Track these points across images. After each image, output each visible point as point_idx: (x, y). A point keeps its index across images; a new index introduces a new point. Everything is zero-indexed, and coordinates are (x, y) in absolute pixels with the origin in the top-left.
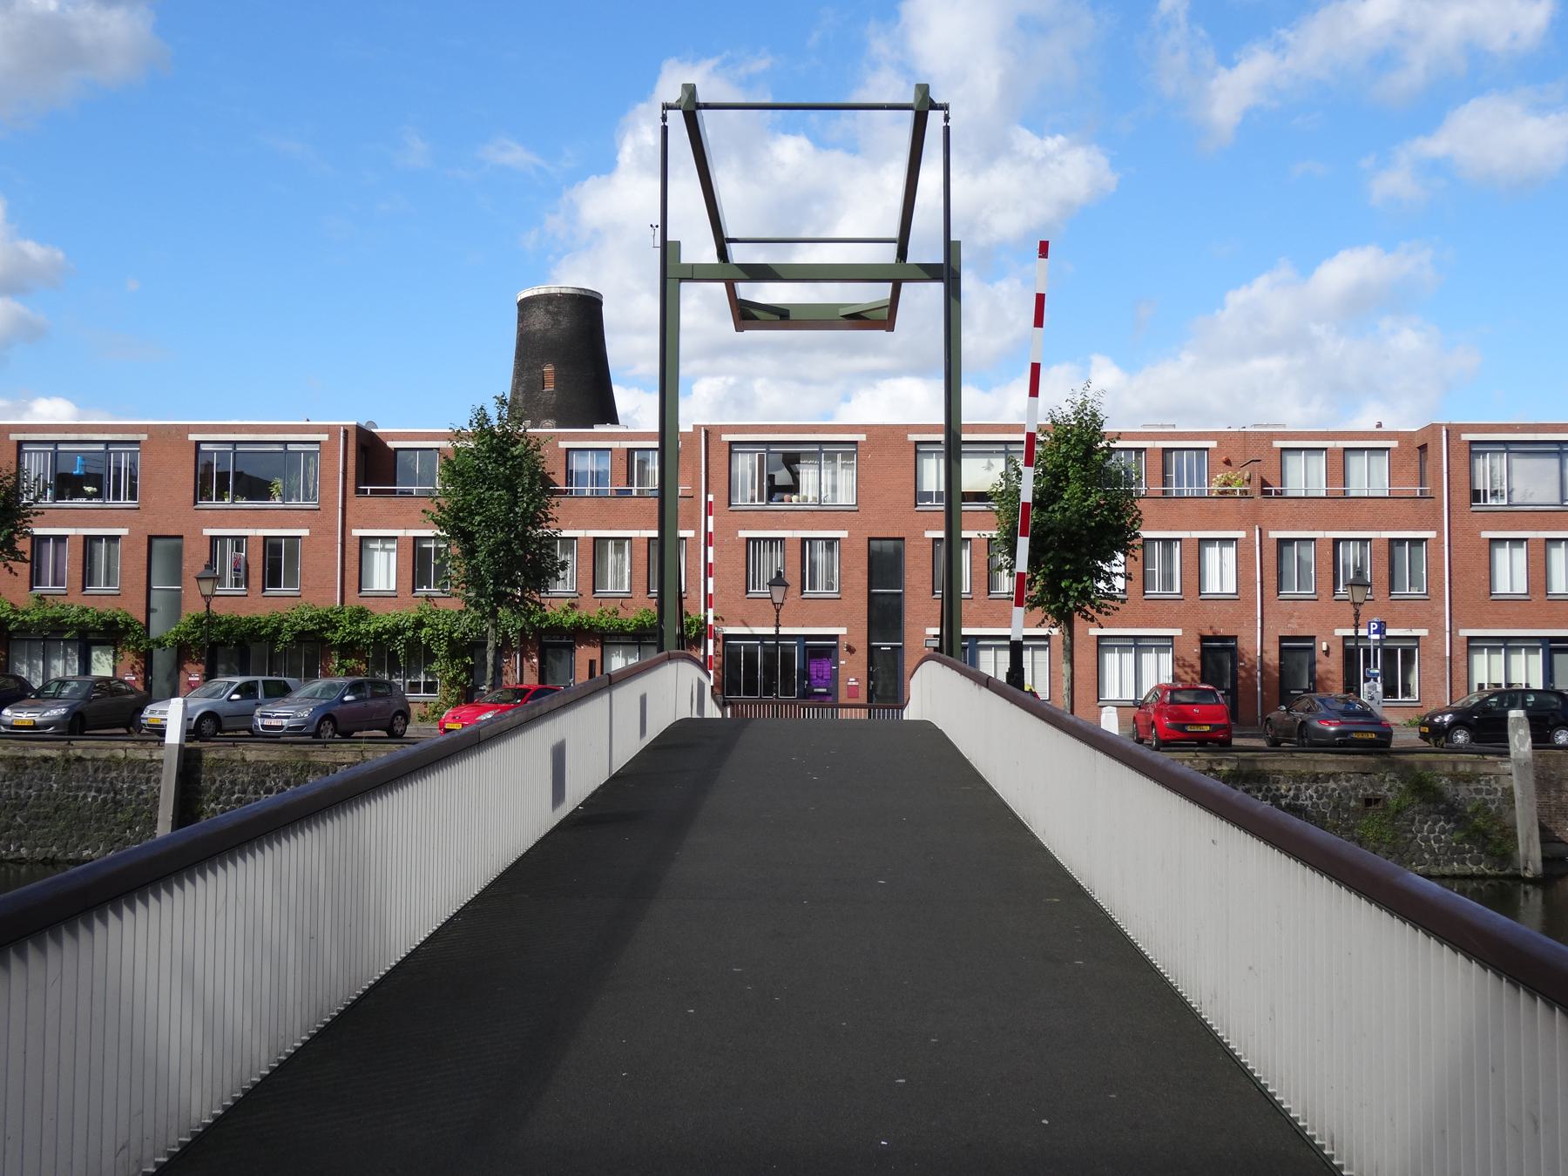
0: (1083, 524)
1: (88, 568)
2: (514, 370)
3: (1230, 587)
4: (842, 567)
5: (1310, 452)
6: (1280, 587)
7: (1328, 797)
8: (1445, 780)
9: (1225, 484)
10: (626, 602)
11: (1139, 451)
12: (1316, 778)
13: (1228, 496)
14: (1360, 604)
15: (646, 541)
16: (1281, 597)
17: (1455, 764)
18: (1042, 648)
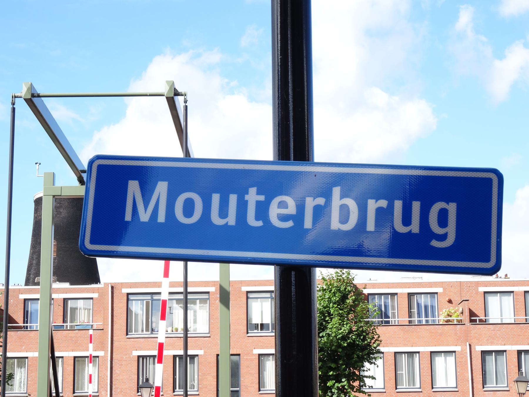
0: (339, 346)
2: (31, 244)
3: (452, 383)
4: (200, 374)
5: (502, 294)
6: (484, 383)
9: (449, 315)
11: (393, 295)
13: (450, 323)
14: (524, 394)
15: (73, 359)
16: (485, 389)
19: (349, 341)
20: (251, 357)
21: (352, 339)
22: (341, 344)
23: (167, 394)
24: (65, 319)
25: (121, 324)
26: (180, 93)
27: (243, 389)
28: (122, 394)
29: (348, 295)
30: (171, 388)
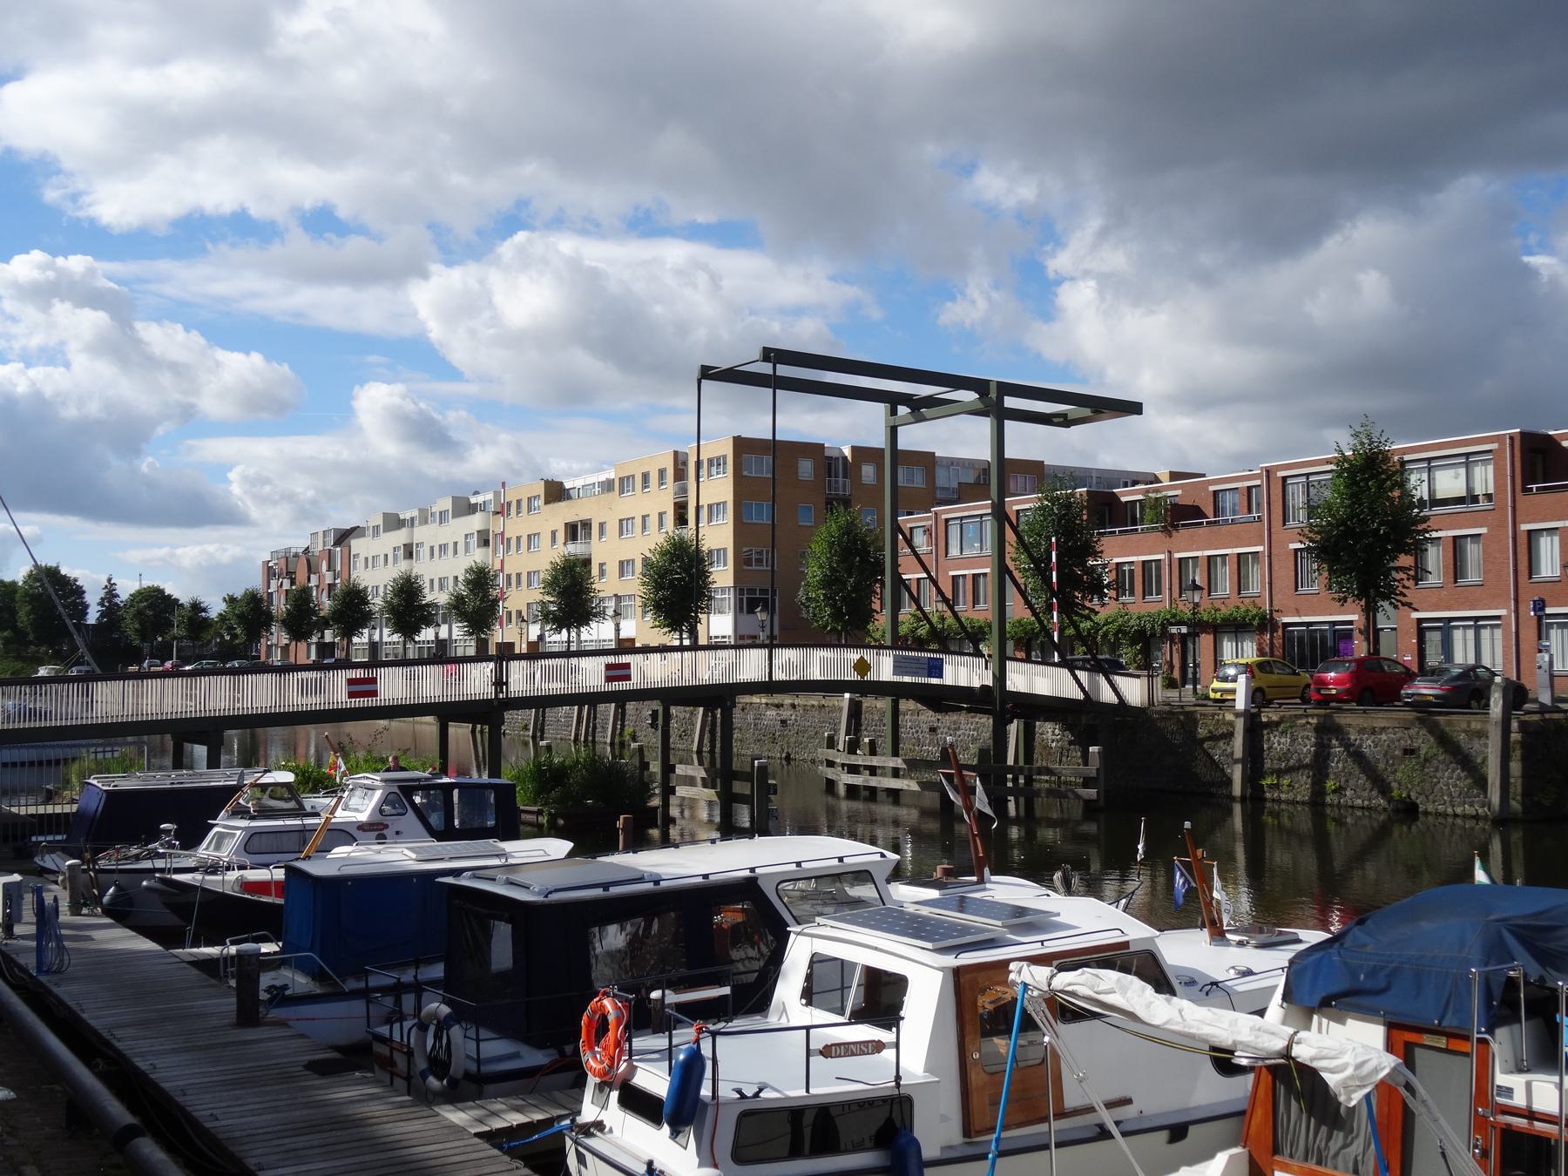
1: (1458, 564)
7: (1381, 746)
8: (1462, 736)
10: (1226, 601)
12: (1373, 731)
17: (1469, 723)
18: (1497, 626)
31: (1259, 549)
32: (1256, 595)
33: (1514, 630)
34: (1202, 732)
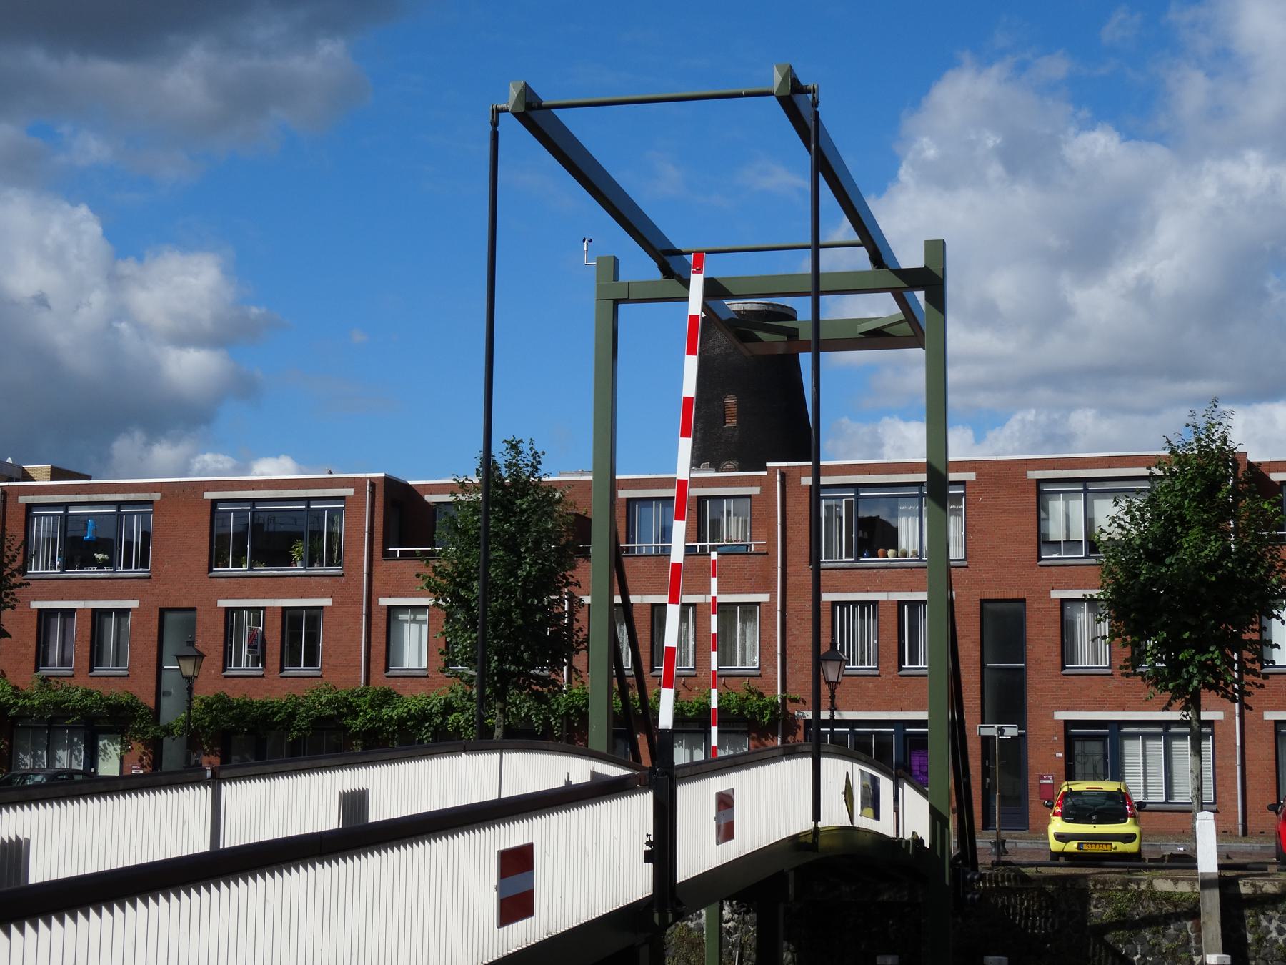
10: (689, 681)
18: (1155, 736)
19: (1220, 572)
20: (1046, 606)
21: (1226, 569)
22: (1205, 578)
23: (887, 674)
24: (702, 535)
25: (799, 543)
26: (805, 88)
27: (1031, 665)
28: (804, 673)
29: (1220, 482)
30: (895, 663)
31: (764, 598)
32: (871, 672)
33: (1238, 743)
34: (1099, 912)
